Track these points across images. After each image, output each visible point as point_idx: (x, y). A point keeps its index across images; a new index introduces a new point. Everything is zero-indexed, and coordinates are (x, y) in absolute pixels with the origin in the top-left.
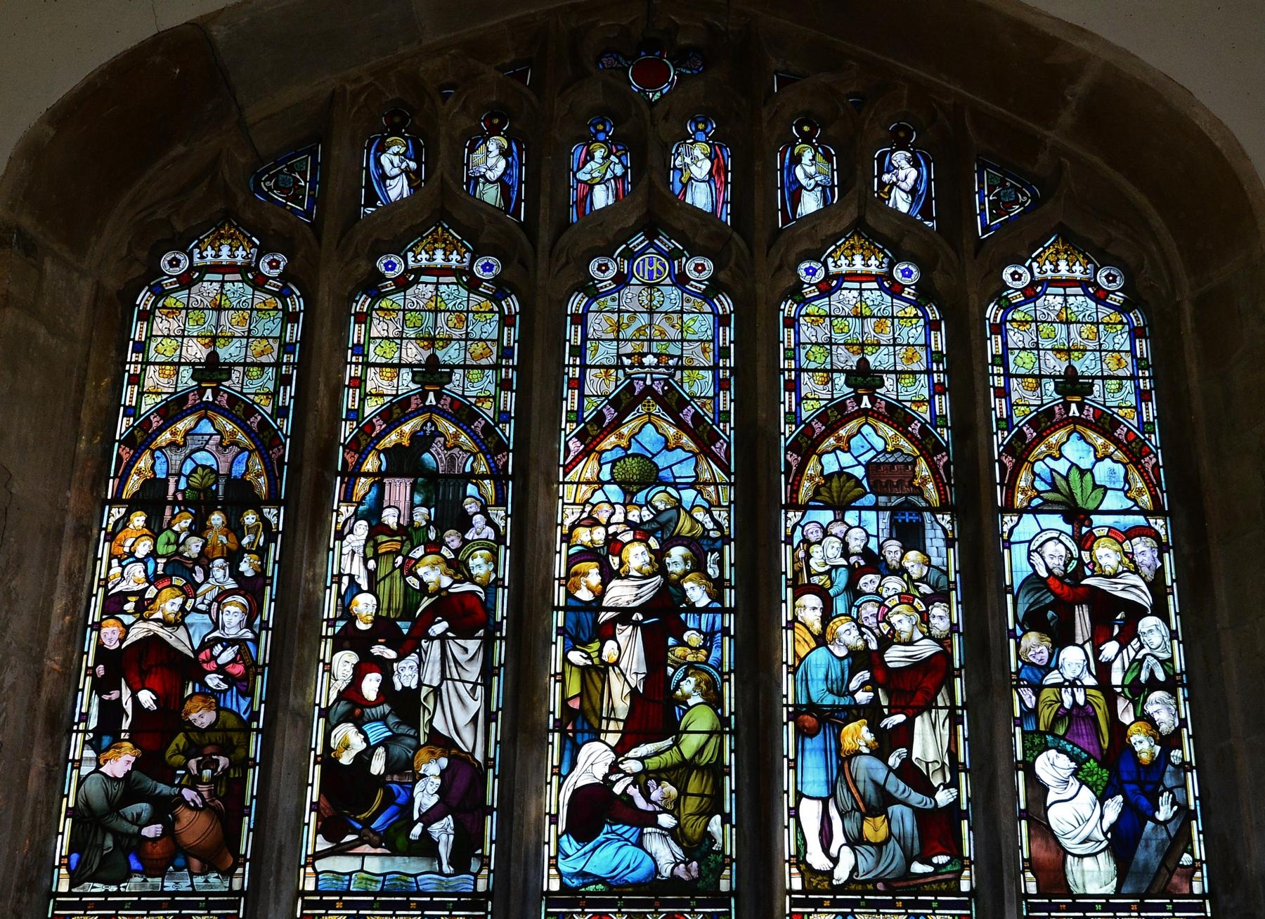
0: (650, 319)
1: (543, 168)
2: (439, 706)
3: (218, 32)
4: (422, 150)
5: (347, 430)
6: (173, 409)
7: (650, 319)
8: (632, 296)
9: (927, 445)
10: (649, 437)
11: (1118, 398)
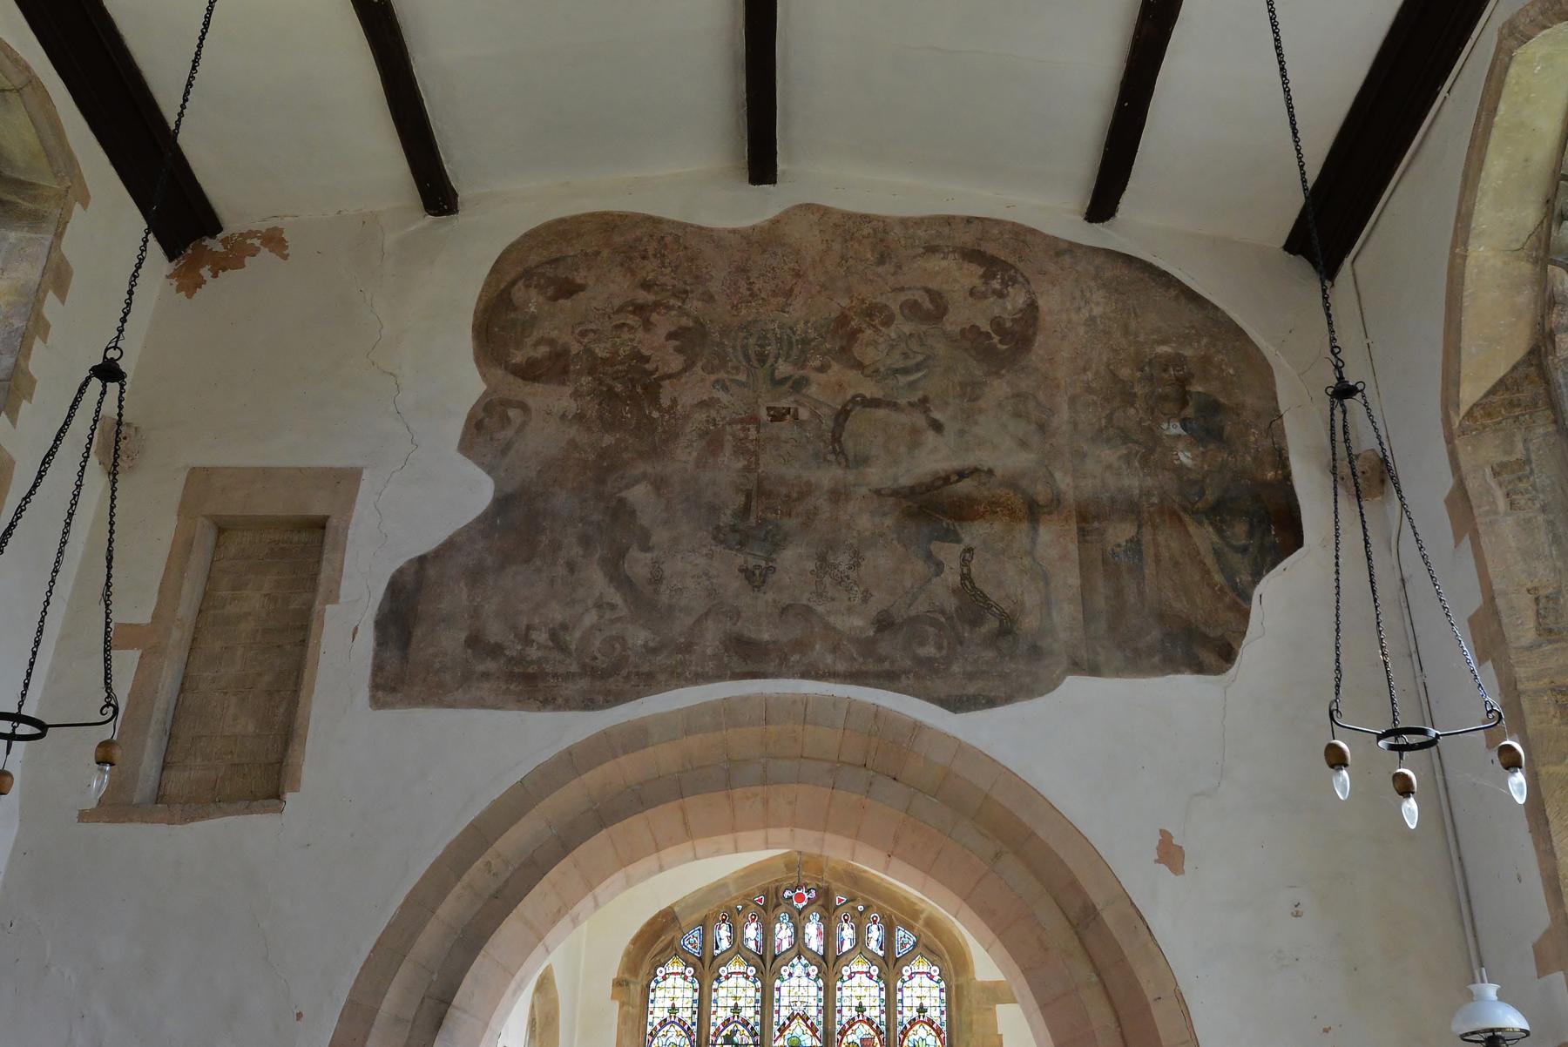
0: (798, 988)
1: (767, 933)
2: (1405, 518)
3: (676, 909)
4: (732, 929)
5: (712, 1029)
6: (664, 1023)
7: (798, 988)
8: (794, 981)
9: (878, 1032)
10: (798, 1032)
11: (933, 1014)
